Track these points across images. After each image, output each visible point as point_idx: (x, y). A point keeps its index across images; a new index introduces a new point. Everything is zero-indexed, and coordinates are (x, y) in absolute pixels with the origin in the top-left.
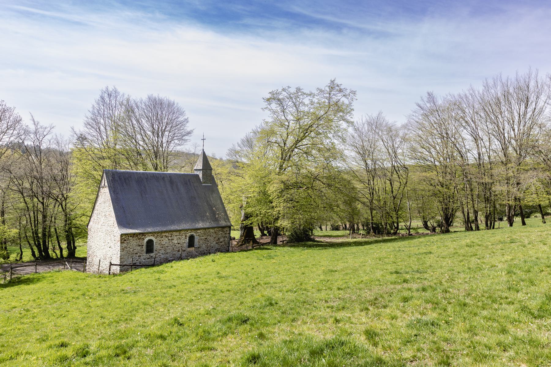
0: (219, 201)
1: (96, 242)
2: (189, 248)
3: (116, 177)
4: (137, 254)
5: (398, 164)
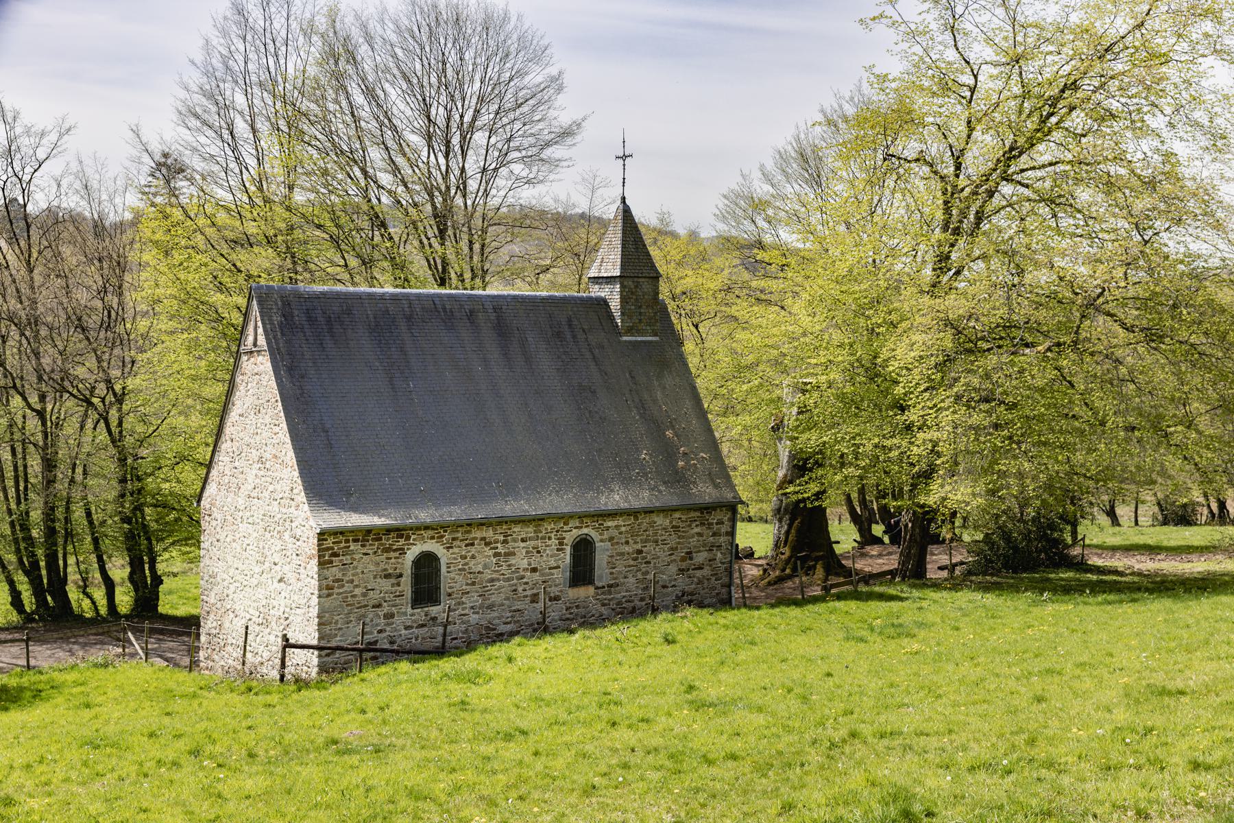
0: (688, 404)
1: (229, 558)
3: (296, 313)
4: (379, 606)
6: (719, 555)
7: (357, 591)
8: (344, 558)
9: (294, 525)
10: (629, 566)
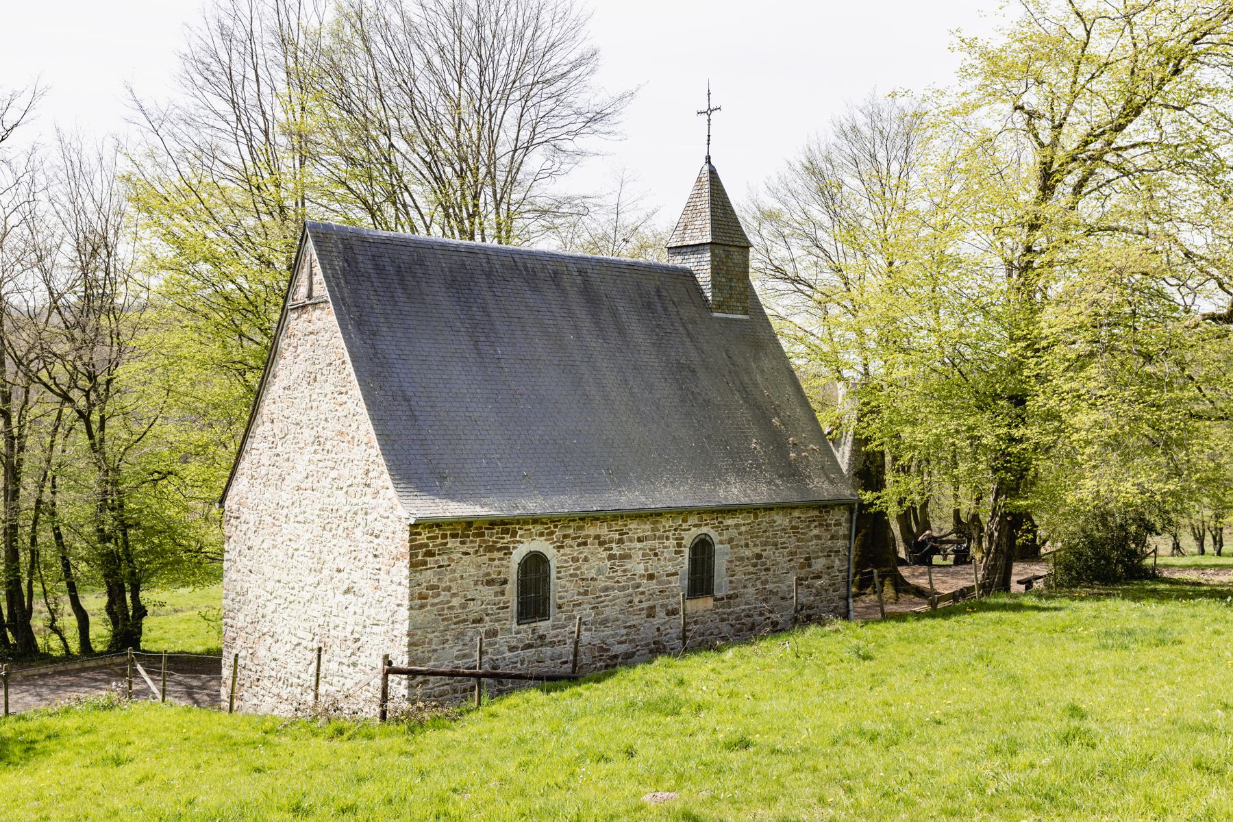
0: (789, 390)
1: (267, 569)
2: (694, 601)
3: (360, 258)
4: (480, 621)
6: (837, 562)
7: (456, 602)
8: (440, 558)
9: (370, 518)
10: (749, 573)
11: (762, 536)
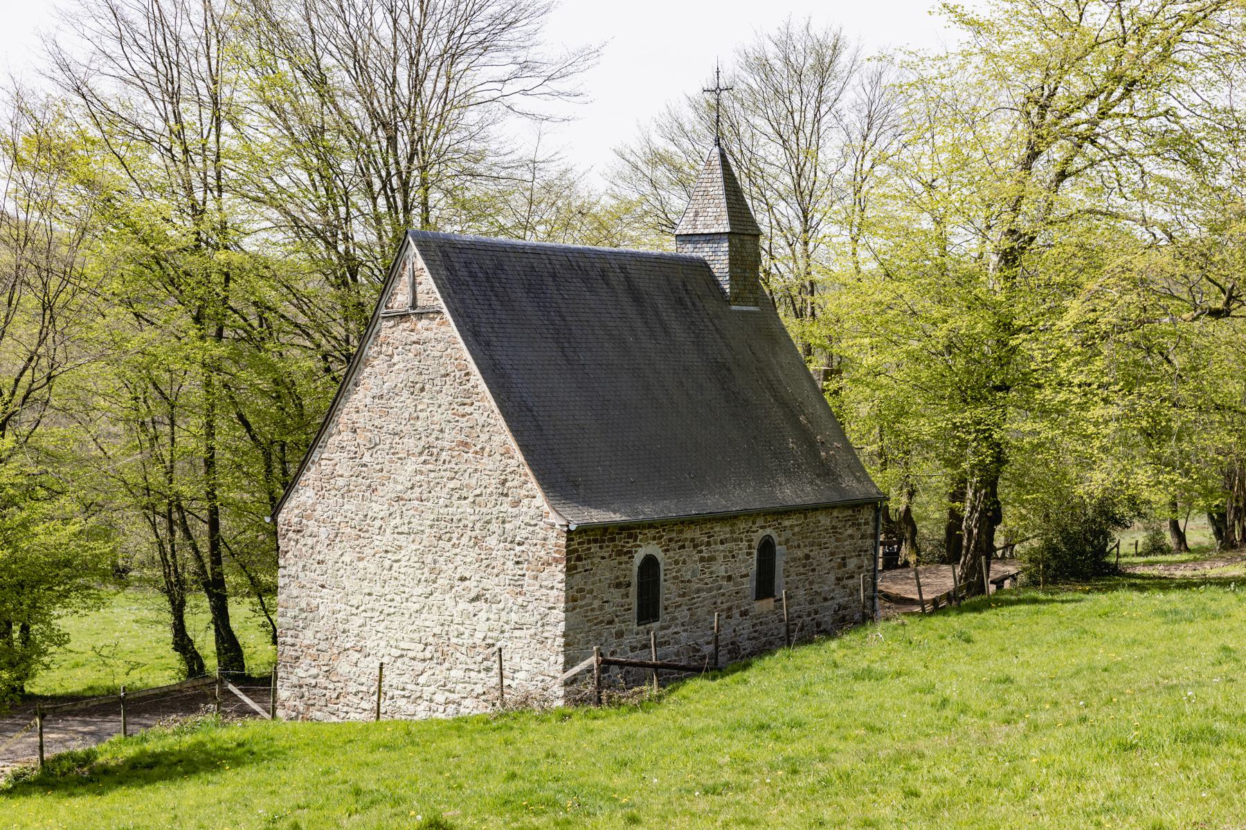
0: (806, 385)
4: (611, 622)
5: (152, 519)
6: (866, 562)
7: (596, 604)
11: (810, 537)
